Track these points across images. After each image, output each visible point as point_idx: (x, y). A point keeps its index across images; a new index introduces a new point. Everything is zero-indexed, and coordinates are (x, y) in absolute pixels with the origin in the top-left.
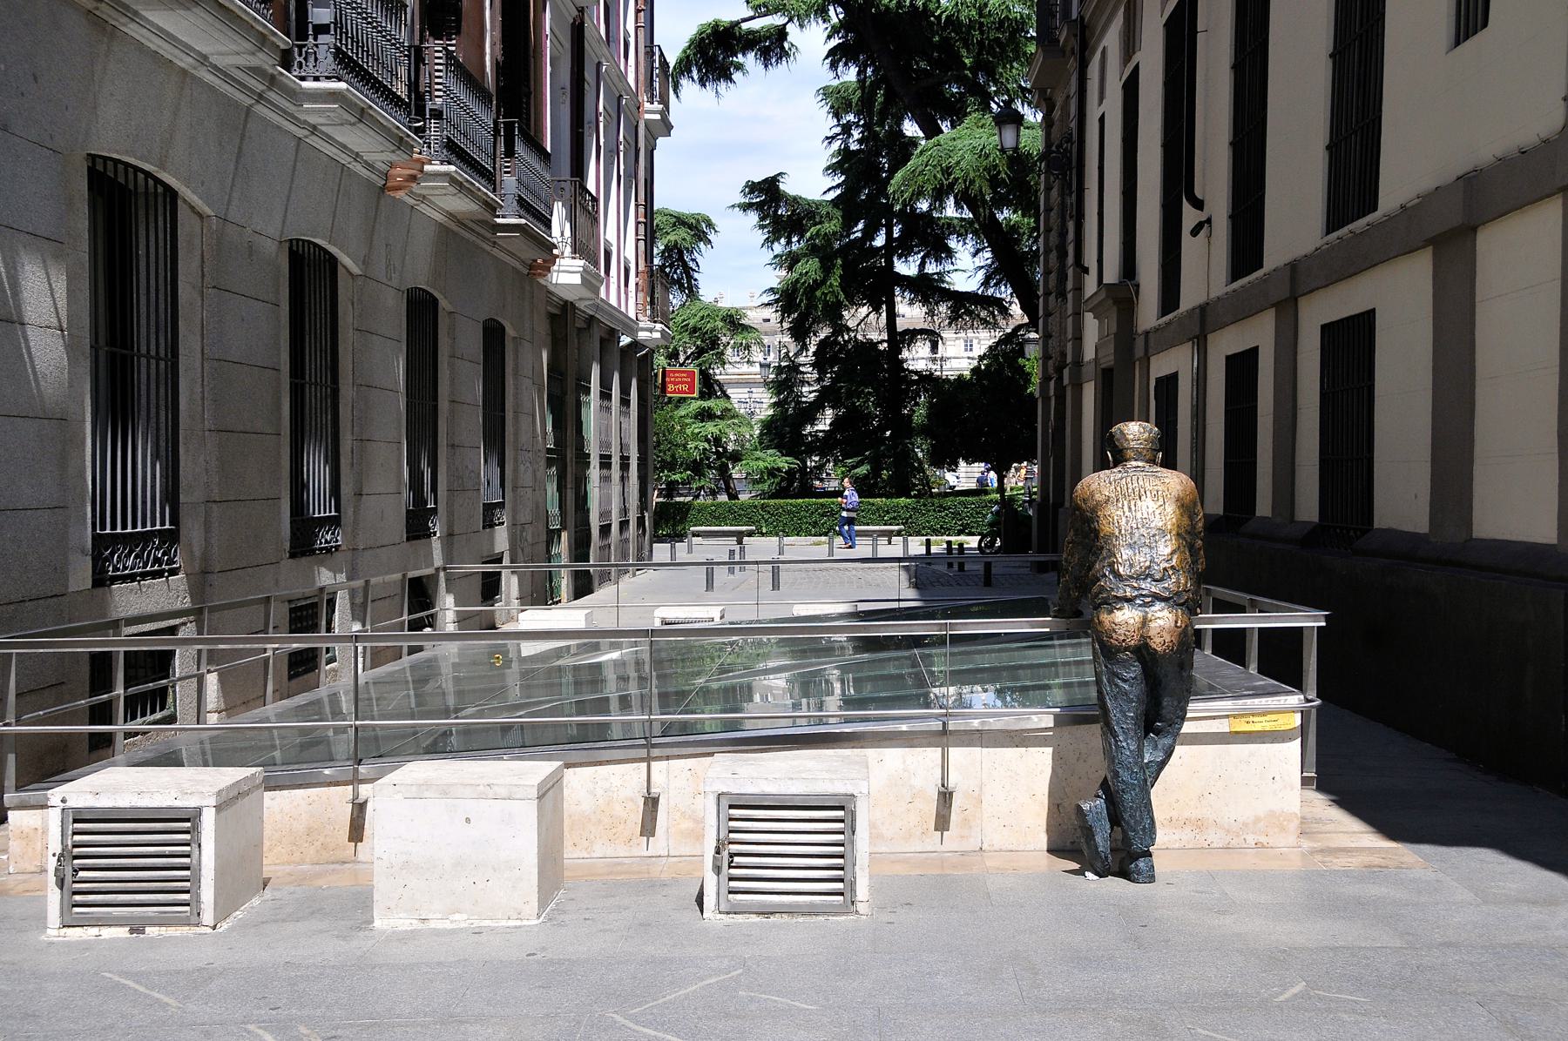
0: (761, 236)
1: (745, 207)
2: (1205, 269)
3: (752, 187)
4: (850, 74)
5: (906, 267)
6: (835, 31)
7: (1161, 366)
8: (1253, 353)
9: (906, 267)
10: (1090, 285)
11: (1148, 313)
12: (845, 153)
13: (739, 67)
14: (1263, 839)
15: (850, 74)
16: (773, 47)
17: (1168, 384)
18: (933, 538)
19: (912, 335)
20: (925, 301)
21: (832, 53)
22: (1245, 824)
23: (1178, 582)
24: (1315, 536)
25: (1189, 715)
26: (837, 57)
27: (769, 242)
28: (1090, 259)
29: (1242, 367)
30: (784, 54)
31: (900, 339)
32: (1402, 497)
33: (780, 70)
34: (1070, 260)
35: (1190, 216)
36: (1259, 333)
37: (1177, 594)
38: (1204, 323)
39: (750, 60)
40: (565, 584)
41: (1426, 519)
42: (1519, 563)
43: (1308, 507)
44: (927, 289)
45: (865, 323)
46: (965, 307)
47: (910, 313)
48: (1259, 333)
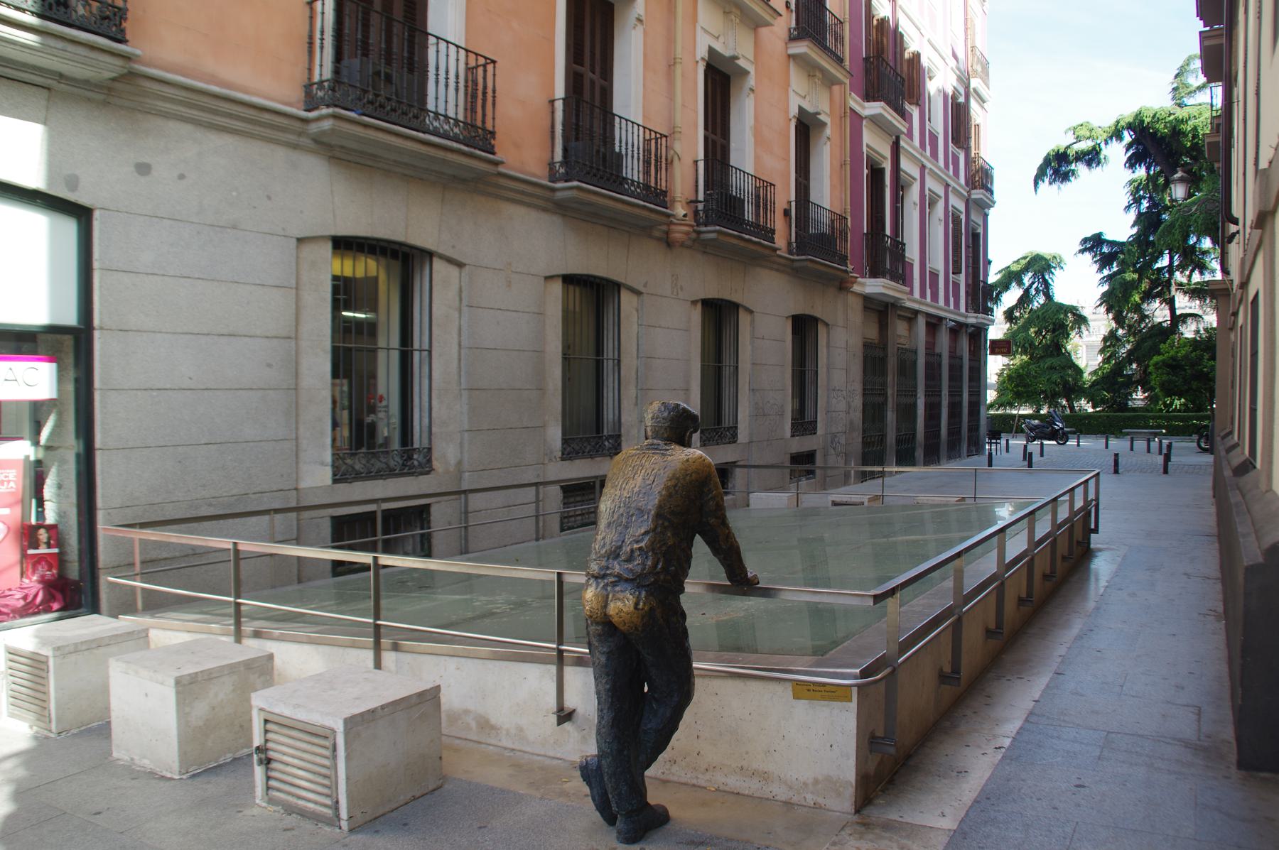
0: (1096, 267)
1: (1082, 251)
3: (1085, 241)
4: (1141, 172)
6: (1129, 147)
12: (1140, 215)
13: (1073, 172)
14: (820, 800)
16: (1092, 157)
18: (1046, 442)
19: (1184, 317)
20: (1199, 298)
21: (1129, 159)
22: (805, 784)
23: (643, 564)
26: (1132, 163)
27: (1101, 269)
31: (1178, 320)
33: (1097, 171)
37: (641, 576)
39: (1081, 168)
40: (919, 453)
45: (1158, 312)
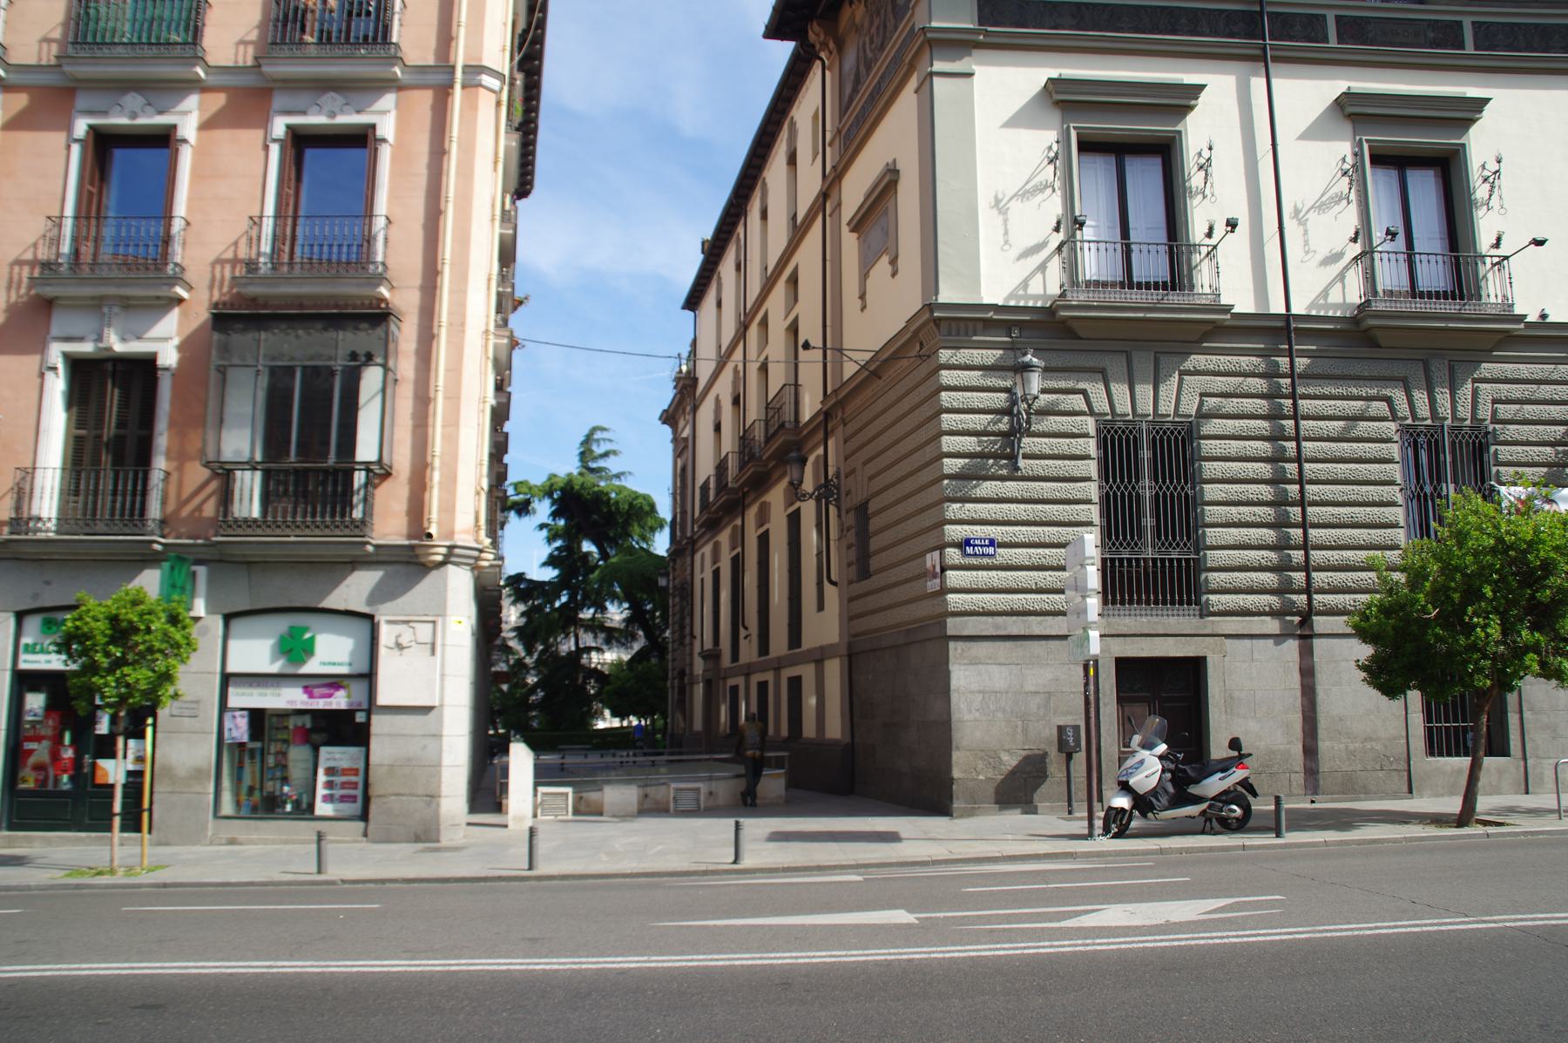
2: (749, 652)
4: (562, 522)
5: (587, 614)
7: (731, 682)
8: (766, 683)
9: (587, 614)
10: (697, 649)
11: (726, 660)
15: (562, 522)
17: (735, 689)
24: (787, 740)
25: (1277, 307)
28: (697, 631)
29: (763, 686)
30: (528, 512)
32: (809, 730)
33: (526, 520)
34: (688, 630)
35: (743, 633)
36: (769, 676)
38: (748, 671)
41: (836, 631)
42: (834, 743)
43: (785, 732)
44: (595, 626)
46: (613, 637)
47: (587, 639)
48: (769, 676)
